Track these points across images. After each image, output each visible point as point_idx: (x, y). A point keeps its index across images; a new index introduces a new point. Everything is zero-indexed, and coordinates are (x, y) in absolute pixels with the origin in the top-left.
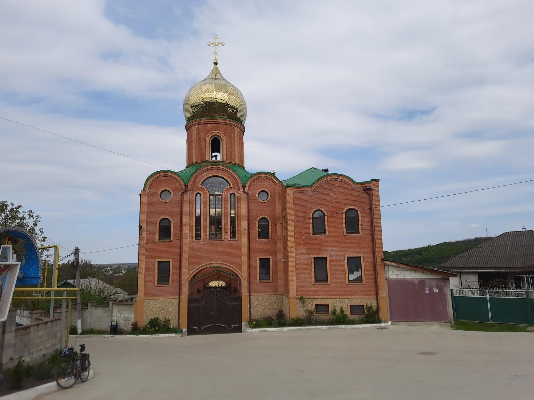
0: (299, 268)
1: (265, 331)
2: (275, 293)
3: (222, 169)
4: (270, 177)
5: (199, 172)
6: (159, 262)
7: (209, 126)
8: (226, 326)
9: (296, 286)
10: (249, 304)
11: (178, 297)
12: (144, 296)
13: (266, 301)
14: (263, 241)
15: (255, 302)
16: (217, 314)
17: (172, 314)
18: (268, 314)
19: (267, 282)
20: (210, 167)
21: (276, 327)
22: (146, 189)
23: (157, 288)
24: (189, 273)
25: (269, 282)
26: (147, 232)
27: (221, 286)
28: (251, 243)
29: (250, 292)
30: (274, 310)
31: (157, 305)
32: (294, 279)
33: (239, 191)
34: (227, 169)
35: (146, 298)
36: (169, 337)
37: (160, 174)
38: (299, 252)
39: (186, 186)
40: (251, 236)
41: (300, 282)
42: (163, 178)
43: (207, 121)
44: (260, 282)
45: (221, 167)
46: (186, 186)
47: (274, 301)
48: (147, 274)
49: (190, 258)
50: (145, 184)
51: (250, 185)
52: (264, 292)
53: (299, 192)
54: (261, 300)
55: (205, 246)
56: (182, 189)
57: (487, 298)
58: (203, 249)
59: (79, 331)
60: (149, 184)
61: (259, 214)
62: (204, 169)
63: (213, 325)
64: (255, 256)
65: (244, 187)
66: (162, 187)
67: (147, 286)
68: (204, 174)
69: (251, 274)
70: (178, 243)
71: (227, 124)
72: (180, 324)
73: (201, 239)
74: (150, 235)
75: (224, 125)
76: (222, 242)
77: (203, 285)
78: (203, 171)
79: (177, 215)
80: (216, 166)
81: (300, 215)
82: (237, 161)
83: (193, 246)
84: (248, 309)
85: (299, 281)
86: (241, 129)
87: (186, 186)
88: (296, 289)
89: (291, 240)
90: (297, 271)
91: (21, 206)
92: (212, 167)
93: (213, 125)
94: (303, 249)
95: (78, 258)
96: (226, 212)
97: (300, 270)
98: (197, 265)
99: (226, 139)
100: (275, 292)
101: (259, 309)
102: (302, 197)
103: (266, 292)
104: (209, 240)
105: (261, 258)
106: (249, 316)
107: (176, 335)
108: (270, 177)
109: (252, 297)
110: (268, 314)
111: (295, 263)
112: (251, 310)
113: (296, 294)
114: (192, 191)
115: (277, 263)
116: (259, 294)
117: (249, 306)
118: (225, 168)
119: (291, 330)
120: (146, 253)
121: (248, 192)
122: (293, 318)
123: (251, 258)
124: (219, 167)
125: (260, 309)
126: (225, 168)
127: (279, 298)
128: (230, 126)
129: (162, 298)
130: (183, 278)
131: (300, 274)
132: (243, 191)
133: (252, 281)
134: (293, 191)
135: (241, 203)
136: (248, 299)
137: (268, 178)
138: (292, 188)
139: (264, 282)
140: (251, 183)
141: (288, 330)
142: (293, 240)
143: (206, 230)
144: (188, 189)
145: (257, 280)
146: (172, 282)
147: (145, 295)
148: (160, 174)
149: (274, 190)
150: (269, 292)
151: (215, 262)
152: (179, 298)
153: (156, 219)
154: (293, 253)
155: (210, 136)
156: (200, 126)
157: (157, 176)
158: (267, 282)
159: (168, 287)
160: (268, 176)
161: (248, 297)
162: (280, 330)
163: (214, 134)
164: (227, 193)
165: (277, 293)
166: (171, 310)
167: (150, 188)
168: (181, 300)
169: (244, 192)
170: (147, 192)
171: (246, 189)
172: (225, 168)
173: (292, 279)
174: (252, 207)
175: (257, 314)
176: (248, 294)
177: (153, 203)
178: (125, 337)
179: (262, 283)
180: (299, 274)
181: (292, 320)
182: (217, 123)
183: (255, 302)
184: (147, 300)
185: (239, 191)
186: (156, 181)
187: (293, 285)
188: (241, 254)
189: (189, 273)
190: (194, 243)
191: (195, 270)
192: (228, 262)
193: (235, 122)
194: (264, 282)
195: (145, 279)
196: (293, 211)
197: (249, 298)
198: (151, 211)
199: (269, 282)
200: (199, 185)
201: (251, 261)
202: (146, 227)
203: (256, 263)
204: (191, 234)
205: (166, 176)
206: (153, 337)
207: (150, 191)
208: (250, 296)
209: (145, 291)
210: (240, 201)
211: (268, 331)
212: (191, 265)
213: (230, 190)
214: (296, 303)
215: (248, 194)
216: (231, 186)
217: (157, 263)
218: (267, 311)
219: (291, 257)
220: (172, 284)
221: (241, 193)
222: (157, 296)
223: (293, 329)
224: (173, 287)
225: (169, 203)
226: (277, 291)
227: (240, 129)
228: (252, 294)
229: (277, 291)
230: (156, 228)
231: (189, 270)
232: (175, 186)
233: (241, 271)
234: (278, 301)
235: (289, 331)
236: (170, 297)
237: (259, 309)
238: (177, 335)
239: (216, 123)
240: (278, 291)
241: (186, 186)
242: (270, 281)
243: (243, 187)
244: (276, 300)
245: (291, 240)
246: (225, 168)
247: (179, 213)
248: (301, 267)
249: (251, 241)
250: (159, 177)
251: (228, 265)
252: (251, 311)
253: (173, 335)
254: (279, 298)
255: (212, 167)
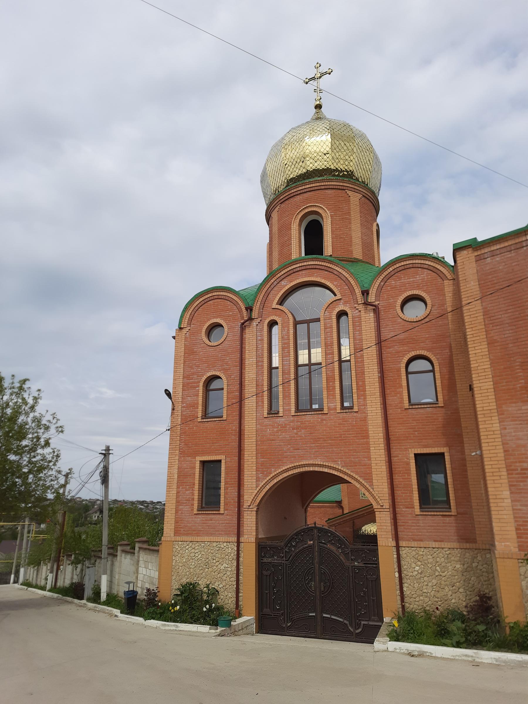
0: (517, 464)
1: (421, 655)
2: (468, 545)
3: (317, 267)
4: (427, 262)
5: (272, 281)
6: (203, 463)
7: (298, 198)
8: (345, 622)
9: (512, 520)
10: (397, 570)
11: (235, 539)
12: (175, 533)
13: (443, 564)
14: (421, 411)
15: (413, 565)
16: (322, 589)
17: (224, 578)
18: (453, 601)
19: (441, 513)
20: (294, 266)
21: (458, 645)
22: (182, 327)
23: (198, 516)
24: (257, 487)
25: (447, 514)
26: (182, 403)
27: (372, 532)
28: (390, 417)
29: (397, 538)
30: (468, 593)
31: (197, 555)
32: (502, 496)
33: (355, 305)
34: (327, 264)
35: (178, 538)
36: (191, 634)
37: (206, 297)
38: (512, 417)
39: (249, 309)
40: (390, 400)
41: (524, 508)
42: (211, 302)
43: (293, 191)
44: (422, 513)
45: (316, 263)
46: (365, 294)
47: (468, 567)
48: (181, 488)
49: (260, 452)
50: (182, 317)
51: (380, 289)
52: (435, 541)
53: (493, 254)
54: (431, 560)
55: (288, 426)
56: (242, 318)
57: (9, 583)
58: (284, 434)
59: (103, 596)
60: (187, 315)
61: (405, 348)
62: (282, 273)
63: (314, 614)
64: (403, 447)
65: (365, 293)
66: (209, 320)
67: (180, 512)
68: (283, 283)
69: (398, 493)
70: (236, 423)
71: (332, 187)
72: (240, 603)
73: (280, 412)
74: (187, 410)
75: (327, 191)
76: (324, 417)
77: (352, 530)
78: (281, 278)
79: (235, 368)
80: (305, 264)
81: (501, 313)
82: (357, 253)
83: (264, 428)
84: (397, 581)
85: (521, 505)
86: (364, 194)
87: (249, 309)
88: (517, 529)
89: (480, 385)
90: (512, 474)
91: (28, 380)
92: (298, 265)
93: (305, 195)
94: (523, 408)
95: (107, 465)
96: (329, 352)
97: (522, 470)
98: (273, 470)
99: (331, 216)
100: (467, 542)
101: (427, 585)
102: (504, 264)
103: (443, 541)
104: (296, 414)
105: (419, 452)
106: (399, 602)
107: (210, 629)
108: (427, 262)
109: (403, 552)
110: (453, 601)
111: (502, 451)
112: (405, 585)
113: (516, 545)
114: (261, 319)
115: (465, 466)
116: (422, 544)
117: (397, 575)
118: (323, 264)
119: (505, 662)
120: (180, 445)
121: (377, 303)
122: (515, 623)
123: (394, 452)
124: (312, 263)
125: (430, 584)
126: (323, 264)
127: (479, 558)
128: (340, 191)
129: (206, 539)
130: (246, 497)
131: (522, 484)
132: (363, 302)
133: (401, 509)
134: (474, 257)
135: (360, 331)
136: (395, 556)
137: (205, 302)
138: (470, 249)
139: (433, 513)
140: (382, 284)
141: (497, 660)
142: (489, 385)
143: (290, 393)
144: (253, 315)
145: (414, 508)
146: (226, 504)
147: (177, 532)
148: (206, 297)
149: (441, 291)
150: (449, 542)
151: (311, 462)
152: (238, 542)
153: (199, 378)
154: (492, 422)
155: (300, 216)
156: (283, 205)
157: (201, 299)
158: (441, 513)
159: (218, 516)
160: (422, 262)
161: (394, 549)
162: (470, 659)
163: (307, 211)
164: (330, 313)
165: (474, 545)
166: (222, 567)
167: (190, 323)
168: (242, 545)
169: (366, 304)
170: (184, 331)
171: (372, 298)
172: (324, 264)
173: (498, 497)
174: (386, 334)
175: (421, 598)
176: (394, 543)
177: (195, 350)
178: (130, 620)
179: (430, 517)
180: (517, 481)
181: (511, 628)
182: (312, 189)
183: (413, 565)
184: (180, 543)
185: (355, 305)
186: (199, 309)
187: (505, 517)
188: (368, 443)
189: (257, 487)
190: (267, 422)
191: (268, 479)
192: (339, 462)
193: (349, 181)
194: (433, 513)
195: (177, 497)
196: (480, 308)
197: (395, 553)
198: (191, 364)
199: (447, 514)
200: (274, 306)
201: (394, 459)
202: (181, 394)
203: (408, 464)
204: (260, 403)
205: (216, 297)
206: (167, 628)
207: (189, 328)
208: (398, 547)
209: (176, 522)
210: (360, 325)
211: (431, 657)
212: (261, 468)
213: (336, 306)
214: (521, 575)
215: (376, 310)
216: (339, 296)
217: (198, 465)
218: (450, 593)
219: (486, 433)
220: (225, 509)
221: (361, 307)
222: (198, 535)
223: (513, 661)
224: (228, 517)
225: (220, 346)
226: (474, 541)
227: (363, 196)
228: (402, 543)
229: (474, 541)
230: (197, 395)
231: (258, 480)
232: (231, 313)
233: (372, 485)
234: (480, 567)
235: (496, 666)
236: (222, 539)
237: (427, 585)
238: (213, 631)
239: (310, 189)
240: (476, 539)
241: (365, 294)
242: (451, 511)
243: (363, 295)
244: (474, 565)
245: (480, 385)
246: (324, 264)
247: (238, 364)
248: (524, 462)
249: (390, 412)
250: (205, 302)
251: (340, 468)
252: (405, 589)
253: (205, 629)
254: (479, 558)
255: (298, 265)
